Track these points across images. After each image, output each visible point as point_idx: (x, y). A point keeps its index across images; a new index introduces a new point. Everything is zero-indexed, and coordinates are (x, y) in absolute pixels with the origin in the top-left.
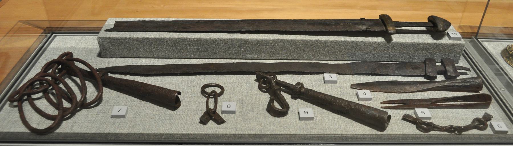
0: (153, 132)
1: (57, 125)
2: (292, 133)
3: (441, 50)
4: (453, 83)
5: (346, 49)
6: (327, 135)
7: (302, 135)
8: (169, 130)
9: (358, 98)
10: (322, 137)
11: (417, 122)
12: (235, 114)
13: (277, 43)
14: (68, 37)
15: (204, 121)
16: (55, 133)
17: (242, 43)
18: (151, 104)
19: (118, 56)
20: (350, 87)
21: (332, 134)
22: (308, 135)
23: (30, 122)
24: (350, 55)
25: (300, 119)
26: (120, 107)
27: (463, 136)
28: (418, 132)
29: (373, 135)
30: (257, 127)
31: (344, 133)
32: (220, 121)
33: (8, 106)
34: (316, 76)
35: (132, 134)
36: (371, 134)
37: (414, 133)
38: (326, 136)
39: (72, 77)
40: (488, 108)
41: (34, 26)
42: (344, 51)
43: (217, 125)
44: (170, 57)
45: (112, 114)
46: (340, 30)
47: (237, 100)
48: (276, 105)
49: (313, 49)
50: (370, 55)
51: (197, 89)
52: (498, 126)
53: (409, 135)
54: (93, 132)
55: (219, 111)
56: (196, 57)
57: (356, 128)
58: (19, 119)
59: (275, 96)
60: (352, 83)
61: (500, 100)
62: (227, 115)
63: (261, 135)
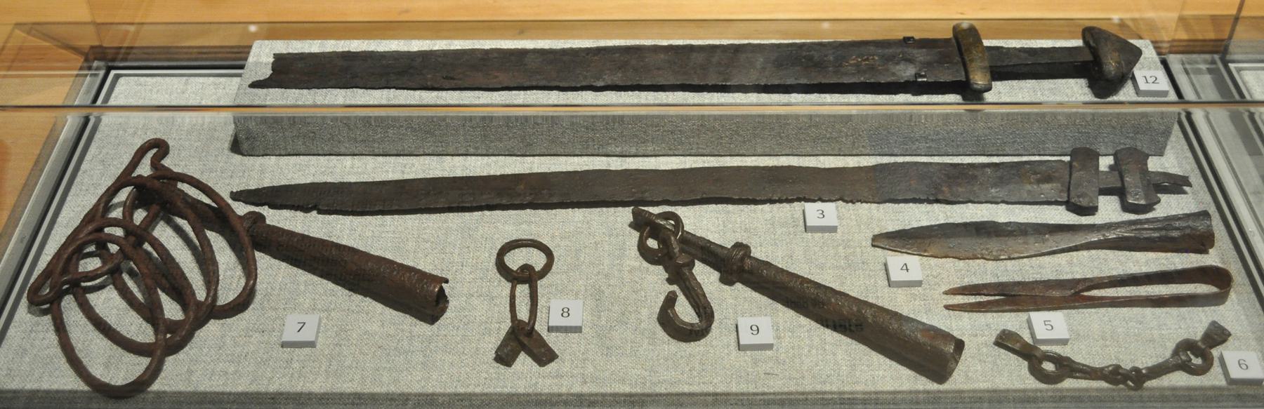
0: (384, 390)
1: (153, 372)
2: (718, 391)
3: (1113, 128)
4: (1136, 232)
5: (863, 131)
6: (803, 393)
7: (743, 394)
8: (423, 383)
9: (889, 281)
10: (791, 399)
11: (1030, 353)
12: (581, 332)
13: (685, 121)
14: (149, 79)
15: (505, 357)
16: (149, 392)
17: (598, 122)
18: (374, 303)
19: (283, 152)
20: (869, 242)
21: (817, 393)
22: (757, 394)
23: (85, 361)
24: (874, 144)
25: (740, 347)
26: (303, 318)
27: (1146, 393)
28: (1032, 383)
29: (918, 392)
30: (633, 372)
31: (847, 388)
32: (544, 356)
33: (26, 310)
34: (786, 207)
35: (335, 394)
36: (912, 389)
37: (1022, 387)
38: (801, 397)
39: (174, 217)
40: (1223, 303)
41: (60, 44)
42: (860, 135)
43: (538, 367)
44: (415, 153)
45: (283, 340)
46: (845, 82)
47: (586, 290)
48: (685, 312)
49: (779, 133)
50: (927, 143)
51: (487, 255)
52: (1240, 365)
53: (1008, 391)
54: (240, 389)
55: (540, 327)
56: (479, 152)
57: (877, 372)
58: (58, 351)
59: (680, 277)
60: (877, 232)
61: (1258, 273)
62: (561, 336)
63: (643, 395)
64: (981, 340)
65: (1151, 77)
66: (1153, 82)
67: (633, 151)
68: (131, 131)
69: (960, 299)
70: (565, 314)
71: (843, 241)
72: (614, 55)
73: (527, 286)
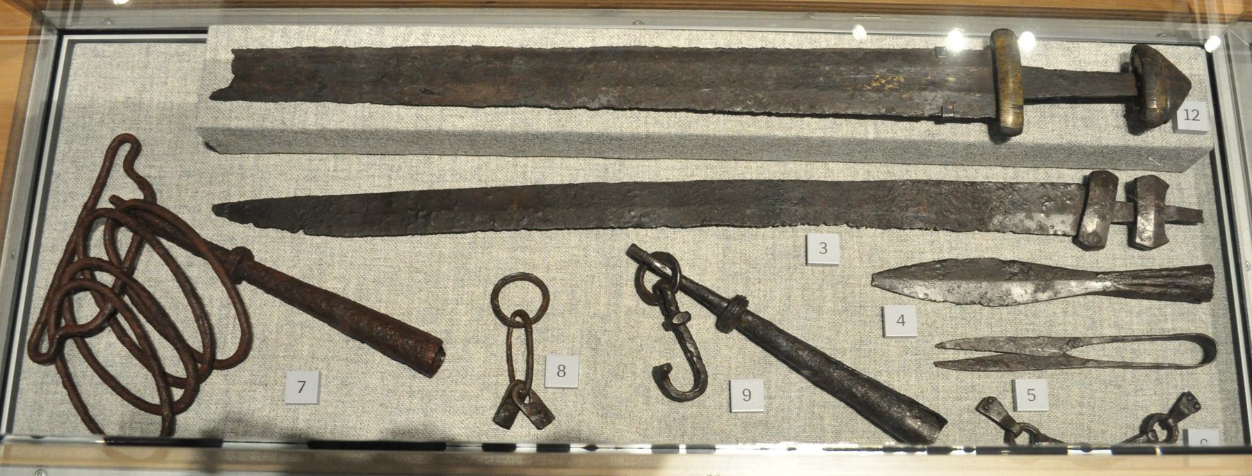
18: (372, 350)
59: (676, 325)
64: (965, 403)
65: (1193, 111)
66: (1194, 119)
67: (627, 156)
68: (98, 117)
69: (951, 355)
70: (561, 373)
71: (843, 277)
72: (610, 64)
73: (523, 329)
